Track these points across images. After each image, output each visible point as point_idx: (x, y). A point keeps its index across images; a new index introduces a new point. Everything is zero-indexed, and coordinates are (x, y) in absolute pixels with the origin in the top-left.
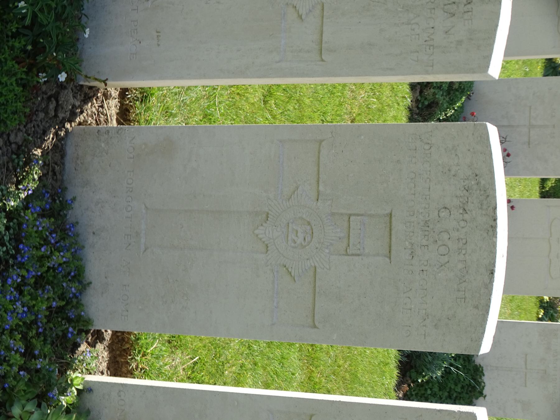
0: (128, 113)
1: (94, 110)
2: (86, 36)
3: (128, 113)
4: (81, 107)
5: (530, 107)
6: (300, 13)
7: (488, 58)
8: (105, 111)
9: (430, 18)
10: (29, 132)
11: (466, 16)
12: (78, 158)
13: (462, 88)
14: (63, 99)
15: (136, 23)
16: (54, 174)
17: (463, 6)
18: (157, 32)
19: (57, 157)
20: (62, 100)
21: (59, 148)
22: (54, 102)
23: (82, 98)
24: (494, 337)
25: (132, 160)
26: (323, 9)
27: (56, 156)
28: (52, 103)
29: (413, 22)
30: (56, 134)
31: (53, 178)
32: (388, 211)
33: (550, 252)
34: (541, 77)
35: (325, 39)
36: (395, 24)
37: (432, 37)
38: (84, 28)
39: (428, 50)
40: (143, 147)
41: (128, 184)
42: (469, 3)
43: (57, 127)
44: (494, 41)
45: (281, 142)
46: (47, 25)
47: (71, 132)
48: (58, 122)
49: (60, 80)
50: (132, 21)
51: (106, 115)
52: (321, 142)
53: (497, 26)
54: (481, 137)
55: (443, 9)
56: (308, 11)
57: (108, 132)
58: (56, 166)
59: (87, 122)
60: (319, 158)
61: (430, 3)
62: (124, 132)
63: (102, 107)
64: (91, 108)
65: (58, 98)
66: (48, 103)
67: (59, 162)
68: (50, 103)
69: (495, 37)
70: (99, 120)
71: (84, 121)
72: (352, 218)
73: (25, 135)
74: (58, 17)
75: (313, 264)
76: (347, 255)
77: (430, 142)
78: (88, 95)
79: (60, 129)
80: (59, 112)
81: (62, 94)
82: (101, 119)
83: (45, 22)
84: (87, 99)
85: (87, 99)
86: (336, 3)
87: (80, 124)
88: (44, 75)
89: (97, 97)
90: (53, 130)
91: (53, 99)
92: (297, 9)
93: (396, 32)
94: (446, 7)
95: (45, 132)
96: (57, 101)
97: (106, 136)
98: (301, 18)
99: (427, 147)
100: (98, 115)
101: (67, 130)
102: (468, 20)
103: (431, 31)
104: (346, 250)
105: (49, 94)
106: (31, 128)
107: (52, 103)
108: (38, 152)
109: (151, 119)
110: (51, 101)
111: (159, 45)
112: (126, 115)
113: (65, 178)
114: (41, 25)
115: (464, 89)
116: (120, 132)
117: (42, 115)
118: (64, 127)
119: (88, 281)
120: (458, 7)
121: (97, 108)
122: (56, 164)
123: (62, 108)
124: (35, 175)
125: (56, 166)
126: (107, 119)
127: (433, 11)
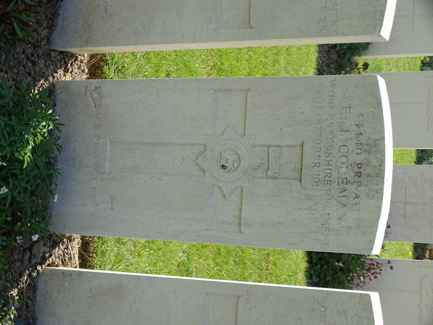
0: (88, 246)
1: (60, 252)
2: (56, 200)
3: (88, 246)
4: (50, 252)
6: (224, 194)
7: (372, 242)
8: (69, 252)
9: (326, 206)
10: (8, 279)
11: (355, 208)
12: (46, 294)
14: (35, 251)
15: (95, 190)
16: (28, 307)
17: (352, 199)
18: (111, 198)
19: (30, 293)
20: (35, 251)
21: (33, 286)
22: (29, 253)
23: (51, 244)
24: (382, 25)
25: (89, 299)
26: (242, 192)
27: (29, 292)
28: (27, 254)
29: (312, 208)
30: (30, 275)
31: (26, 310)
33: (421, 302)
34: (413, 164)
35: (243, 215)
36: (299, 208)
37: (327, 221)
38: (53, 194)
39: (324, 231)
40: (98, 289)
42: (357, 197)
43: (30, 269)
44: (376, 230)
45: (207, 294)
46: (23, 203)
47: (42, 272)
48: (31, 265)
49: (33, 240)
50: (91, 188)
51: (70, 254)
52: (239, 297)
53: (379, 218)
54: (365, 305)
55: (337, 200)
56: (230, 192)
57: (71, 275)
58: (29, 301)
59: (55, 263)
60: (237, 310)
61: (326, 194)
62: (83, 276)
63: (67, 248)
64: (58, 251)
65: (31, 250)
66: (24, 254)
67: (31, 297)
68: (25, 254)
69: (377, 226)
70: (64, 259)
71: (52, 263)
73: (5, 282)
74: (33, 193)
77: (325, 305)
78: (55, 241)
79: (33, 271)
80: (32, 259)
81: (35, 247)
82: (66, 258)
83: (22, 201)
84: (55, 245)
85: (54, 245)
86: (252, 188)
87: (49, 265)
88: (21, 237)
89: (64, 242)
90: (27, 272)
91: (27, 251)
92: (222, 189)
93: (300, 216)
94: (339, 199)
95: (21, 275)
96: (31, 252)
97: (70, 278)
98: (225, 197)
99: (323, 309)
100: (64, 255)
101: (38, 271)
102: (356, 210)
103: (327, 217)
105: (25, 247)
106: (9, 276)
107: (27, 254)
108: (15, 292)
109: (106, 251)
110: (26, 252)
111: (112, 209)
112: (87, 247)
113: (36, 308)
114: (19, 203)
116: (80, 275)
117: (18, 264)
118: (37, 270)
120: (348, 199)
121: (63, 249)
122: (29, 298)
123: (35, 256)
124: (11, 315)
125: (29, 301)
126: (71, 258)
127: (329, 201)
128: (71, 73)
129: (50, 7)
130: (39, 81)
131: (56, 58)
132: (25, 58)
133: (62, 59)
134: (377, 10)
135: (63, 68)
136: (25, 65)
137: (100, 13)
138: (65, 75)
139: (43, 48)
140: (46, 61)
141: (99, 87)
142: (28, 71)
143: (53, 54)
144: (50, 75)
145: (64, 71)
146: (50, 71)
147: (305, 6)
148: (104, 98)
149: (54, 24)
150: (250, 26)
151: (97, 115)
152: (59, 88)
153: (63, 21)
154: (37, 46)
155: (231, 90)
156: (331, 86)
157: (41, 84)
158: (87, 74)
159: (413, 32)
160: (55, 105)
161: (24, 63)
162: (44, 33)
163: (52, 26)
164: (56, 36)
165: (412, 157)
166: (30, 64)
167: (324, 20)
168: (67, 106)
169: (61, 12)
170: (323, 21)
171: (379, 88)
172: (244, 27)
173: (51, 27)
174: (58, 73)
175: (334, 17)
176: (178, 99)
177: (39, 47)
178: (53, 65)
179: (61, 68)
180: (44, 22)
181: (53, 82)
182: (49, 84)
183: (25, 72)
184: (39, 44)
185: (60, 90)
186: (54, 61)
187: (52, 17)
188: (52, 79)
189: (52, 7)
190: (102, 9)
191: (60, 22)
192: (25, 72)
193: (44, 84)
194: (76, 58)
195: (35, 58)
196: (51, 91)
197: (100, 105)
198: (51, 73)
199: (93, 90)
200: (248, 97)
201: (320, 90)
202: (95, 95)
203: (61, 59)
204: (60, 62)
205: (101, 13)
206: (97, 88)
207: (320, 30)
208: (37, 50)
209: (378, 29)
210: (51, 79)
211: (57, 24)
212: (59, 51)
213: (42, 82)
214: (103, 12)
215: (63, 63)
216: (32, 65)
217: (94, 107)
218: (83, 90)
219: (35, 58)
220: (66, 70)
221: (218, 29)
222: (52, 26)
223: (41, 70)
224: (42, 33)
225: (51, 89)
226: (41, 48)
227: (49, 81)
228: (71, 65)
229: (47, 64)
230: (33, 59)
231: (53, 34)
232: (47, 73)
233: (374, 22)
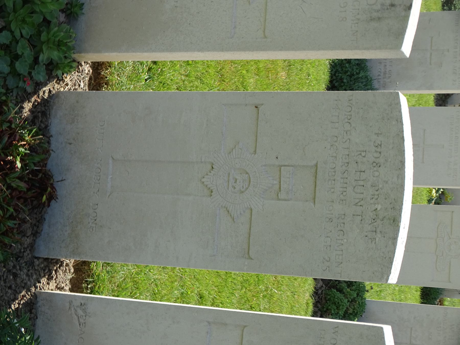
5: (411, 329)
13: (356, 312)
24: (390, 273)
32: (314, 162)
41: (101, 126)
72: (282, 168)
75: (249, 207)
76: (279, 199)
104: (278, 195)
115: (357, 313)
119: (43, 252)
128: (55, 279)
129: (36, 213)
130: (21, 292)
131: (40, 266)
132: (6, 271)
133: (46, 267)
134: (385, 257)
135: (47, 277)
136: (6, 279)
137: (89, 223)
138: (48, 284)
139: (25, 258)
140: (28, 271)
141: (85, 304)
142: (9, 285)
143: (37, 262)
144: (32, 285)
145: (48, 279)
146: (32, 281)
147: (309, 242)
148: (90, 317)
149: (39, 231)
150: (249, 256)
151: (81, 334)
152: (41, 300)
153: (49, 227)
154: (19, 257)
155: (226, 324)
156: (334, 333)
157: (23, 296)
158: (73, 274)
159: (423, 162)
160: (37, 318)
161: (5, 277)
162: (27, 241)
163: (37, 232)
164: (40, 242)
165: (416, 299)
166: (11, 277)
167: (328, 259)
168: (49, 320)
169: (47, 217)
170: (327, 261)
171: (384, 341)
172: (243, 257)
173: (36, 234)
174: (41, 283)
175: (339, 258)
176: (169, 327)
177: (21, 257)
178: (36, 274)
179: (44, 276)
180: (28, 231)
181: (36, 293)
182: (31, 295)
183: (5, 286)
184: (21, 255)
185: (42, 302)
186: (38, 270)
187: (37, 224)
188: (34, 289)
189: (38, 213)
190: (91, 219)
191: (45, 227)
192: (5, 286)
193: (25, 296)
194: (61, 264)
195: (17, 270)
196: (31, 305)
197: (85, 323)
198: (33, 283)
199: (77, 307)
200: (244, 335)
201: (322, 336)
202: (80, 312)
203: (45, 267)
204: (44, 270)
205: (91, 224)
206: (83, 304)
207: (324, 270)
208: (19, 261)
209: (385, 277)
210: (33, 289)
211: (42, 230)
212: (43, 258)
213: (23, 293)
214: (92, 223)
215: (47, 271)
216: (13, 277)
217: (79, 325)
218: (68, 304)
219: (17, 270)
220: (50, 277)
221: (214, 256)
222: (37, 232)
223: (22, 282)
224: (26, 243)
225: (33, 301)
226: (24, 259)
227: (31, 292)
228: (56, 271)
229: (30, 274)
230: (14, 271)
231: (37, 240)
232: (29, 283)
233: (382, 269)
